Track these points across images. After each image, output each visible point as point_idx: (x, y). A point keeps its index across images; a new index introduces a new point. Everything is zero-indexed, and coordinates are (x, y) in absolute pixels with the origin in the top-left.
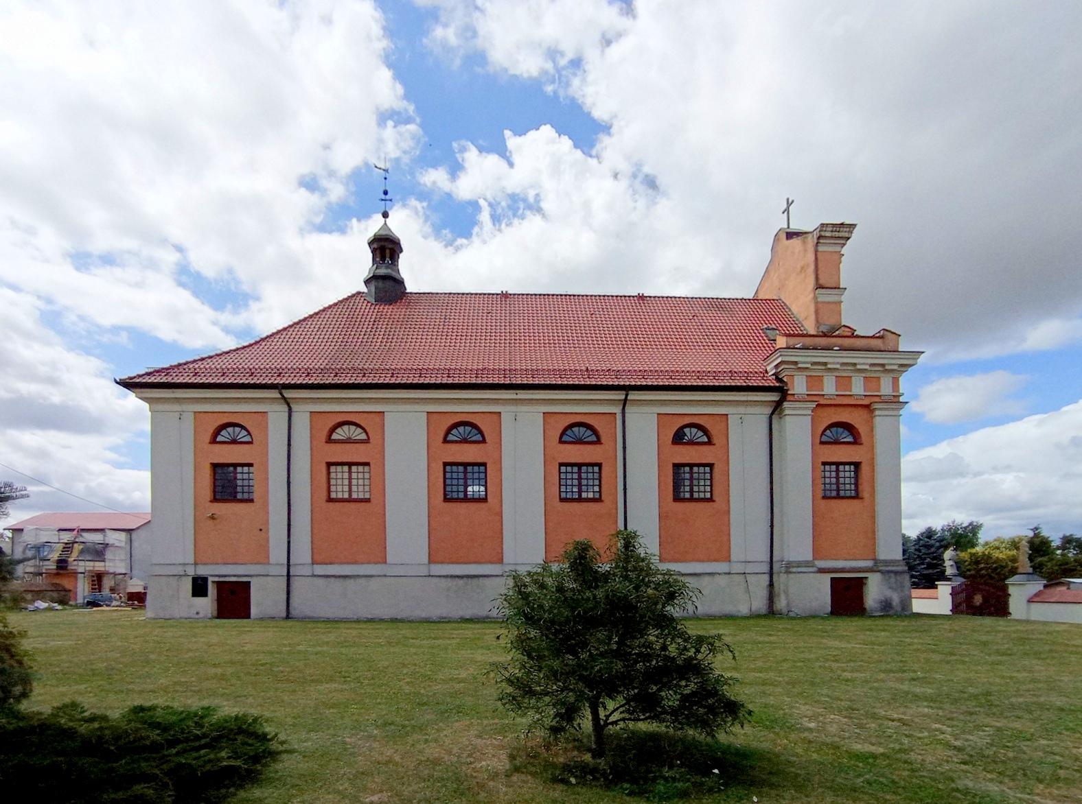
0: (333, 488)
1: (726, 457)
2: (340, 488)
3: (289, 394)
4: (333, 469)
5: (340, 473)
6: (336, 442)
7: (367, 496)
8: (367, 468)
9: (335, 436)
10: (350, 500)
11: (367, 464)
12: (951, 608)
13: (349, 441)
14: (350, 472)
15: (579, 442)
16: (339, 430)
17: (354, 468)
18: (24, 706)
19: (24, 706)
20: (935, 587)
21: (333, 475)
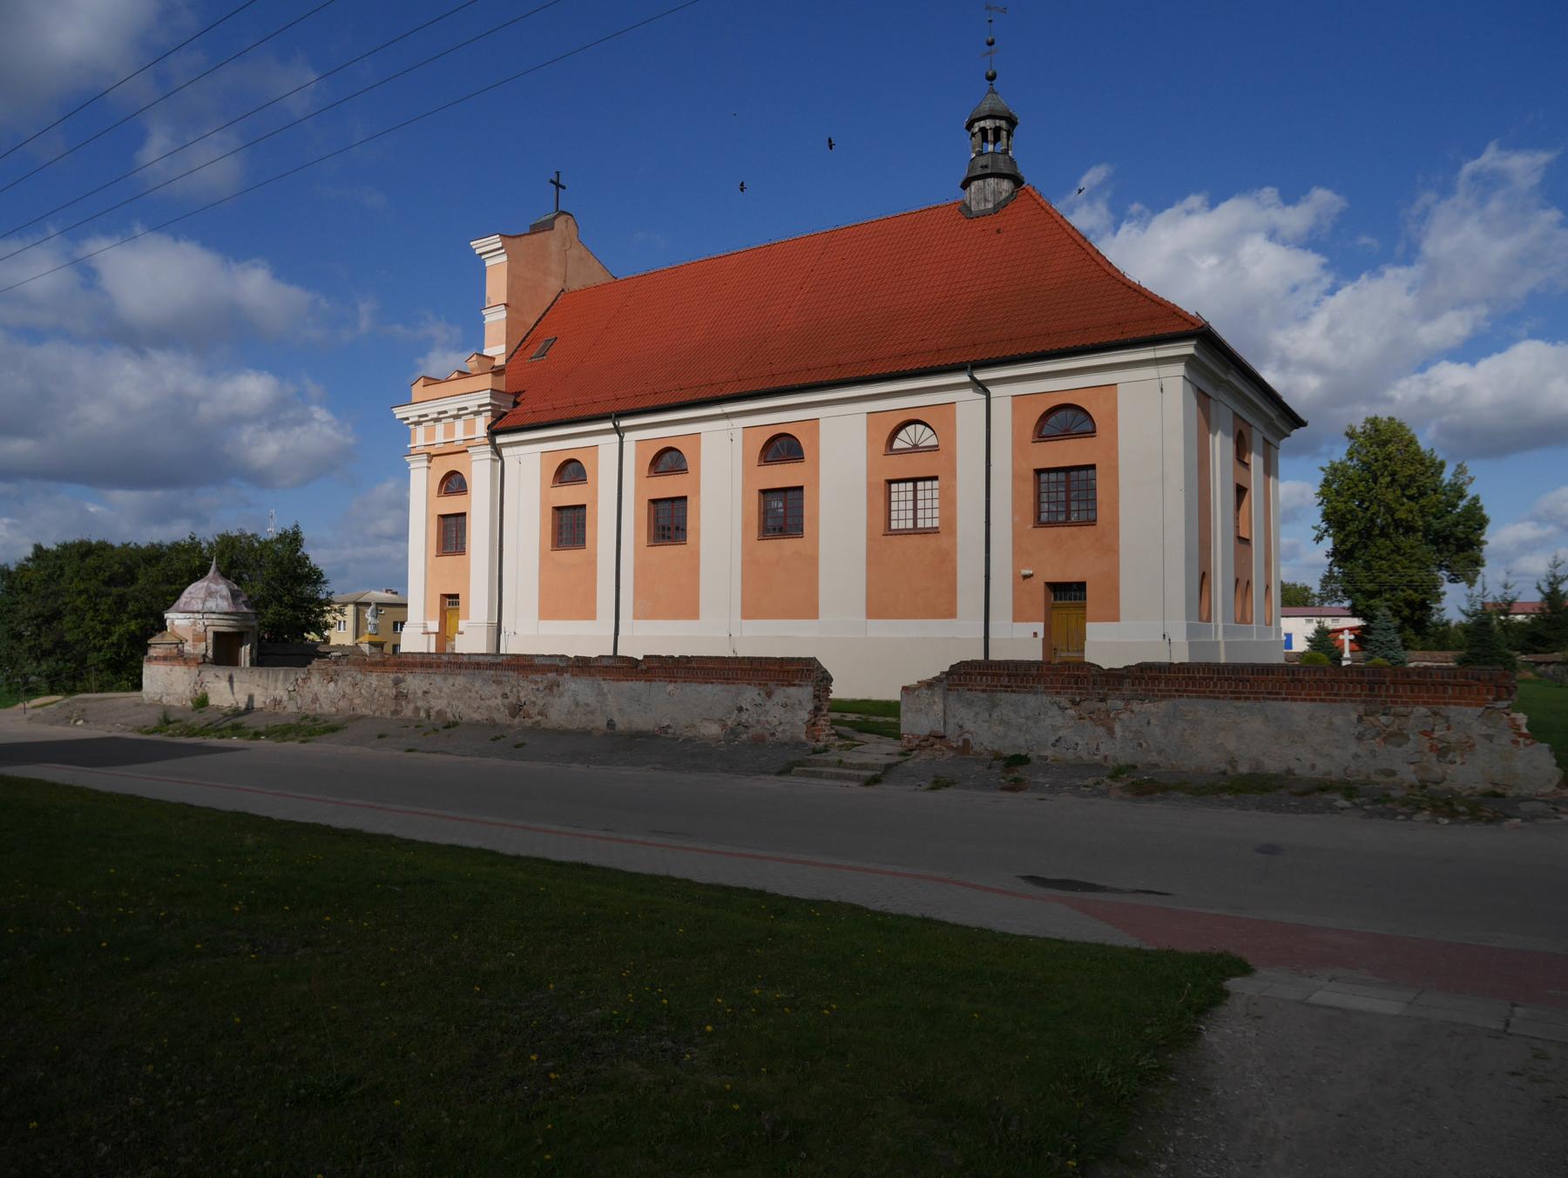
0: (894, 515)
1: (667, 505)
2: (902, 515)
3: (981, 376)
4: (894, 487)
5: (902, 492)
6: (902, 451)
7: (936, 523)
8: (936, 484)
9: (897, 444)
10: (915, 531)
11: (936, 478)
12: (50, 544)
13: (915, 448)
14: (915, 491)
15: (1066, 434)
16: (902, 434)
17: (920, 485)
18: (832, 696)
19: (832, 696)
20: (1227, 994)
21: (894, 497)
